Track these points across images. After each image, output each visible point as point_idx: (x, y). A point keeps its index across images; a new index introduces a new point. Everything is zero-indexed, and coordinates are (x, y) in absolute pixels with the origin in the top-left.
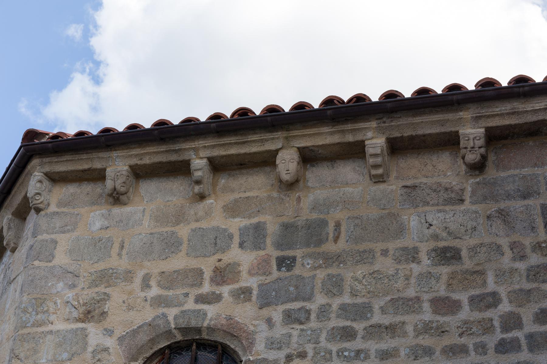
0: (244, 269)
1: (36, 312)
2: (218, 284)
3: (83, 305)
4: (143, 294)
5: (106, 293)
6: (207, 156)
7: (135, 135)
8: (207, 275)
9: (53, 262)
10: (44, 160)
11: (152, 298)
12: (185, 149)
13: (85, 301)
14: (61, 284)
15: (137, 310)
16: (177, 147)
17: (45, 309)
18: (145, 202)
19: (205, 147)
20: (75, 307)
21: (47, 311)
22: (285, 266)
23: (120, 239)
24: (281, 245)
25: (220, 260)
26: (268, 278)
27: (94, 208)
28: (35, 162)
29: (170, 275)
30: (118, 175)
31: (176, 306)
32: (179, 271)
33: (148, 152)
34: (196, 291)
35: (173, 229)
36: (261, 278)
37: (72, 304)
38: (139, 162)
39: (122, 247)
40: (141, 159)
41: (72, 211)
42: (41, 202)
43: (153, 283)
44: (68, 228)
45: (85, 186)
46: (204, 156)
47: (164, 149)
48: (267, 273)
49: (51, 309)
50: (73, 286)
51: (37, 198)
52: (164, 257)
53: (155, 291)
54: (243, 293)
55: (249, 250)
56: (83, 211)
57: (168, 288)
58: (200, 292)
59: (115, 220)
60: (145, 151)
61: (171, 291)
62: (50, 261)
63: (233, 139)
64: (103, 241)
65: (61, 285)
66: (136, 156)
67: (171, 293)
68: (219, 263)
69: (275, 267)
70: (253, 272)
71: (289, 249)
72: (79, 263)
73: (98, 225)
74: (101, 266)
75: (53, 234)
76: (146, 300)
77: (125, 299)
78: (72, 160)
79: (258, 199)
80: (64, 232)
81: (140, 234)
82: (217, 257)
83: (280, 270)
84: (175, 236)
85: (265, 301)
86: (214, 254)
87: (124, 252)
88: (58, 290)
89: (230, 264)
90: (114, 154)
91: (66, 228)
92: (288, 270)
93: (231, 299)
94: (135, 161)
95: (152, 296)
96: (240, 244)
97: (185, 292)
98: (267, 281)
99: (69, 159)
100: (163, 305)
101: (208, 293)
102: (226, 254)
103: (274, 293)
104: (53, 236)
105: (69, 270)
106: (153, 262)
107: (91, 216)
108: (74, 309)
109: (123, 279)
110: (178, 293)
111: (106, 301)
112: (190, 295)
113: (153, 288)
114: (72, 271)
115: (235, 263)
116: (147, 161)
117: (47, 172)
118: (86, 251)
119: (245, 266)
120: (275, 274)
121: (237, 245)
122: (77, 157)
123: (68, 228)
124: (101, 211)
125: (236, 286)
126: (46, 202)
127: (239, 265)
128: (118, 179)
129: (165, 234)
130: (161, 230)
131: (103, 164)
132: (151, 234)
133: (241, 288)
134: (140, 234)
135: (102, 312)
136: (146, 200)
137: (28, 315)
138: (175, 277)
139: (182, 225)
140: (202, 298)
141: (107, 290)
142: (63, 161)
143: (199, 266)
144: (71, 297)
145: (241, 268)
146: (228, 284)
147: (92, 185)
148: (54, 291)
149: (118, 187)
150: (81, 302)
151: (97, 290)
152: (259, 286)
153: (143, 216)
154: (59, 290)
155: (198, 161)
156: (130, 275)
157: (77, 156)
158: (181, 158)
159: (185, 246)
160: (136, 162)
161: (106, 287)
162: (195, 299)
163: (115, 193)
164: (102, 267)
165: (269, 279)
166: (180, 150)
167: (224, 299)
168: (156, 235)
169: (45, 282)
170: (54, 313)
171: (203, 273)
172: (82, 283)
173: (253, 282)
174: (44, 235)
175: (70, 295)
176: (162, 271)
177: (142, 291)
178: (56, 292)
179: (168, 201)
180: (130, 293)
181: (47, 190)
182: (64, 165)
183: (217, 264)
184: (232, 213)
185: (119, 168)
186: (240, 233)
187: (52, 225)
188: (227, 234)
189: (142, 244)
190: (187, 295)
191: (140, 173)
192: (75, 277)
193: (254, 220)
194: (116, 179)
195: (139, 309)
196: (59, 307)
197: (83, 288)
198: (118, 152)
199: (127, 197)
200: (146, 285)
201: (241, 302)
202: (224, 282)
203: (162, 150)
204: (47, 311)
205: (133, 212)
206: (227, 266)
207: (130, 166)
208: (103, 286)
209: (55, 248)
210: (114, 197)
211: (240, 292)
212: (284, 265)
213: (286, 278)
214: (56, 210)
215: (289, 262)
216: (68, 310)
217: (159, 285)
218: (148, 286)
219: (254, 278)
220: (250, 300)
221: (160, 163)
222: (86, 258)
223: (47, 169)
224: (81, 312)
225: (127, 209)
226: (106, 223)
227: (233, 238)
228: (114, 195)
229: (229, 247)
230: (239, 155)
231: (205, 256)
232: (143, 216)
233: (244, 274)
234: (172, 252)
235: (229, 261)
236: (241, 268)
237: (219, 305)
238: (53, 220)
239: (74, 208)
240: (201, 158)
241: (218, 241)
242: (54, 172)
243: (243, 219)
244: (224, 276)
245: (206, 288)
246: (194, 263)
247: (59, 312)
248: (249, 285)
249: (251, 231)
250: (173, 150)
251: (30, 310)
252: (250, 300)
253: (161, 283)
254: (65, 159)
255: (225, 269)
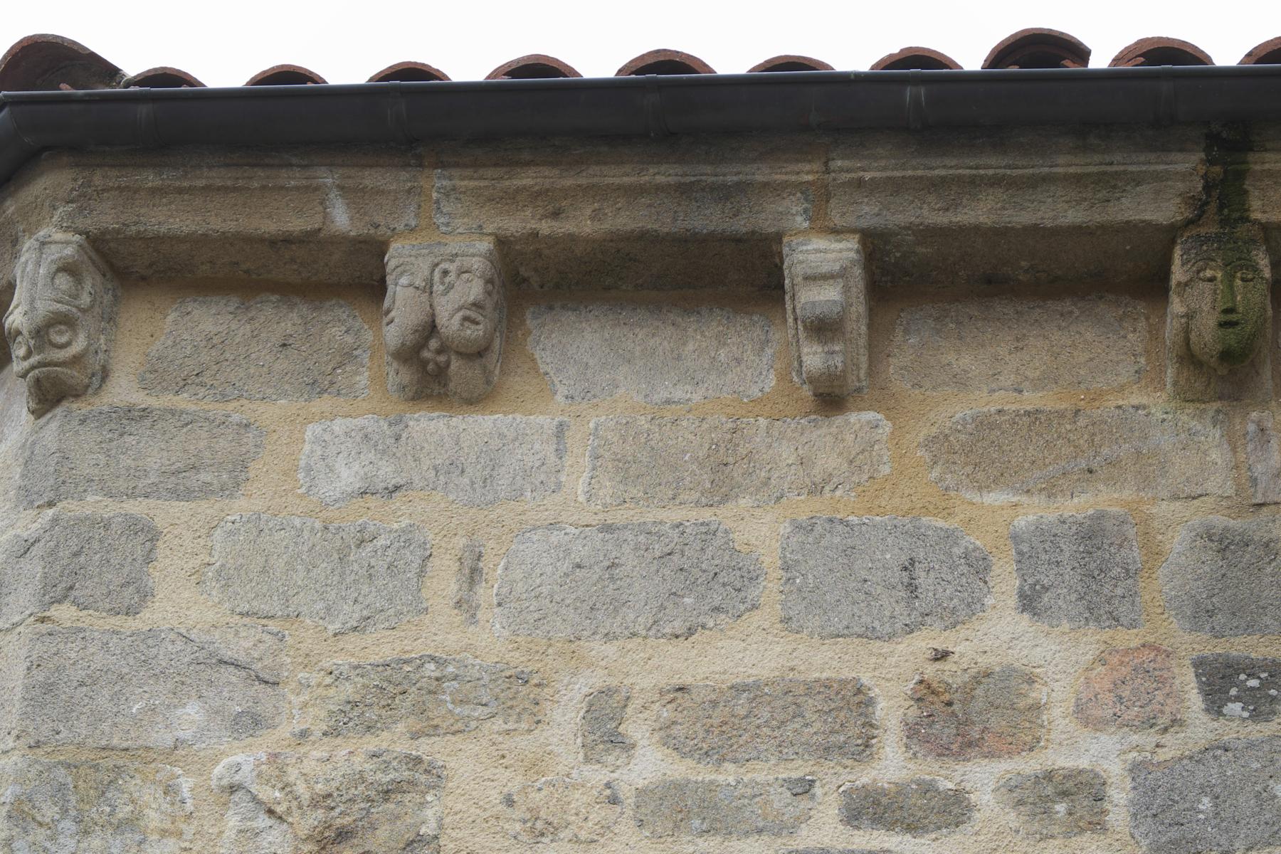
0: (1057, 696)
1: (78, 821)
2: (943, 752)
3: (315, 804)
4: (597, 776)
5: (418, 760)
6: (864, 223)
7: (533, 112)
8: (891, 710)
9: (145, 614)
10: (98, 180)
11: (640, 792)
12: (766, 185)
13: (320, 788)
14: (188, 709)
15: (576, 840)
16: (731, 174)
17: (124, 811)
18: (559, 398)
19: (860, 183)
20: (271, 812)
21: (131, 823)
22: (1237, 699)
23: (461, 542)
24: (1211, 613)
25: (941, 656)
26: (1167, 739)
27: (323, 404)
28: (49, 184)
29: (714, 704)
30: (445, 273)
31: (760, 831)
32: (757, 685)
33: (592, 186)
34: (845, 776)
35: (707, 515)
36: (1135, 738)
37: (254, 798)
38: (545, 227)
39: (473, 575)
40: (556, 215)
41: (217, 410)
42: (76, 360)
43: (636, 729)
44: (205, 477)
45: (269, 311)
46: (851, 221)
47: (672, 180)
48: (1163, 721)
49: (152, 814)
50: (250, 723)
51: (63, 339)
52: (679, 626)
53: (649, 764)
54: (1065, 794)
55: (1066, 626)
56: (269, 412)
57: (714, 755)
58: (865, 780)
59: (426, 463)
60: (583, 181)
61: (729, 766)
62: (131, 611)
63: (992, 164)
64: (381, 542)
65: (192, 712)
66: (536, 196)
67: (728, 775)
68: (938, 665)
69: (1195, 700)
70: (1097, 713)
71: (1249, 629)
72: (273, 626)
73: (348, 476)
74: (381, 646)
75: (132, 495)
76: (614, 800)
77: (514, 787)
78: (235, 189)
79: (1082, 422)
80: (176, 494)
81: (552, 526)
82: (924, 642)
83: (1220, 713)
84: (718, 541)
85: (1174, 833)
86: (909, 629)
87: (485, 594)
88: (181, 734)
89: (988, 675)
90: (436, 182)
91: (195, 480)
92: (1256, 716)
93: (1012, 818)
94: (516, 223)
95: (641, 783)
96: (1022, 595)
97: (795, 775)
98: (1162, 755)
99: (219, 183)
100: (696, 823)
101: (901, 789)
102: (963, 632)
103: (1206, 803)
104: (136, 507)
105: (228, 655)
106: (631, 645)
107: (308, 434)
108: (263, 821)
109: (494, 704)
110: (761, 777)
111: (424, 793)
112: (818, 790)
113: (638, 752)
114: (242, 658)
115: (1009, 673)
116: (583, 223)
117: (104, 232)
118: (299, 577)
119: (1056, 686)
120: (1200, 727)
121: (1013, 601)
122: (259, 178)
123: (205, 477)
124: (359, 422)
125: (1029, 765)
126: (95, 363)
127: (1031, 680)
128: (451, 287)
129: (675, 534)
130: (649, 518)
131: (378, 219)
132: (607, 528)
133: (1049, 776)
134: (552, 526)
135: (411, 836)
136: (562, 390)
137: (41, 834)
138: (743, 712)
139: (745, 502)
140: (876, 803)
141: (424, 748)
142: (190, 190)
143: (847, 674)
144: (246, 768)
145: (1039, 693)
146: (990, 755)
147: (304, 309)
148: (161, 737)
149: (450, 323)
150: (301, 788)
151: (372, 743)
152: (1135, 769)
153: (560, 453)
154: (186, 734)
155: (819, 243)
156: (524, 690)
157: (260, 173)
158: (741, 225)
159: (774, 586)
160: (533, 225)
161: (415, 736)
162: (847, 807)
163: (434, 344)
164: (387, 652)
165: (1173, 746)
166: (742, 188)
167: (977, 815)
168: (628, 535)
169: (114, 697)
170: (164, 833)
171: (871, 702)
172: (298, 710)
173: (1105, 755)
174: (90, 498)
175: (242, 759)
176: (676, 681)
177: (587, 760)
178: (170, 742)
179: (668, 402)
180: (534, 766)
181: (97, 310)
182: (175, 211)
183: (930, 670)
184: (969, 469)
185: (454, 245)
186: (1020, 553)
187: (126, 461)
188: (957, 551)
189: (566, 566)
190: (804, 788)
191: (536, 284)
192: (258, 687)
193: (1079, 505)
194: (438, 288)
195: (583, 835)
196: (189, 806)
197: (304, 734)
198: (456, 172)
199: (484, 369)
200: (605, 730)
201: (1056, 830)
202: (970, 744)
203: (660, 179)
204: (131, 823)
205: (511, 435)
206: (976, 680)
207: (502, 242)
208: (400, 727)
209: (149, 559)
210: (424, 363)
211: (1049, 790)
212: (1233, 692)
213: (1251, 745)
214: (140, 399)
215: (1253, 683)
216: (232, 822)
217: (667, 735)
218: (618, 742)
219: (1104, 737)
220: (1098, 825)
221: (643, 237)
222: (304, 609)
223: (106, 217)
224: (302, 834)
225: (478, 426)
226: (386, 472)
227: (987, 569)
228: (426, 354)
229: (974, 607)
230: (999, 233)
231: (869, 634)
232: (560, 453)
233: (1059, 718)
234: (717, 609)
235: (984, 661)
236: (1039, 693)
237: (958, 837)
238: (127, 439)
239: (224, 398)
240: (836, 232)
241: (922, 579)
242: (140, 237)
243: (1024, 499)
244: (968, 722)
245: (892, 765)
246: (824, 661)
247: (189, 830)
248: (1084, 763)
249: (1068, 548)
250: (713, 188)
251: (49, 812)
252: (1098, 825)
253: (675, 730)
254: (201, 183)
255: (968, 693)
